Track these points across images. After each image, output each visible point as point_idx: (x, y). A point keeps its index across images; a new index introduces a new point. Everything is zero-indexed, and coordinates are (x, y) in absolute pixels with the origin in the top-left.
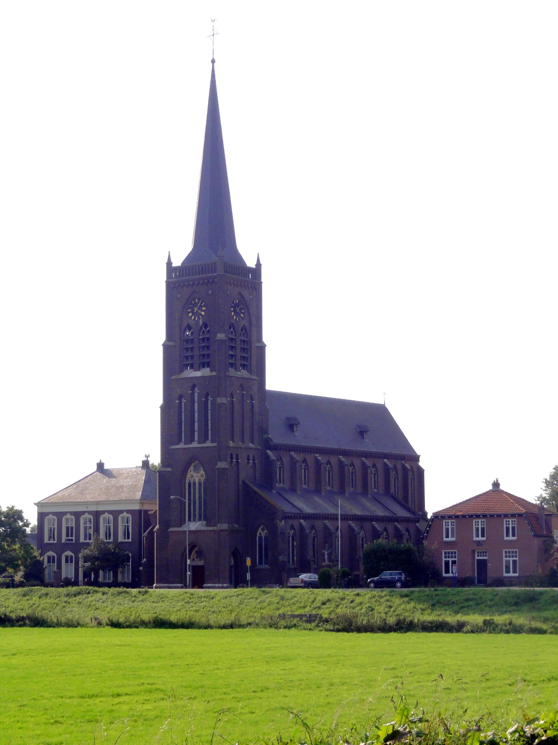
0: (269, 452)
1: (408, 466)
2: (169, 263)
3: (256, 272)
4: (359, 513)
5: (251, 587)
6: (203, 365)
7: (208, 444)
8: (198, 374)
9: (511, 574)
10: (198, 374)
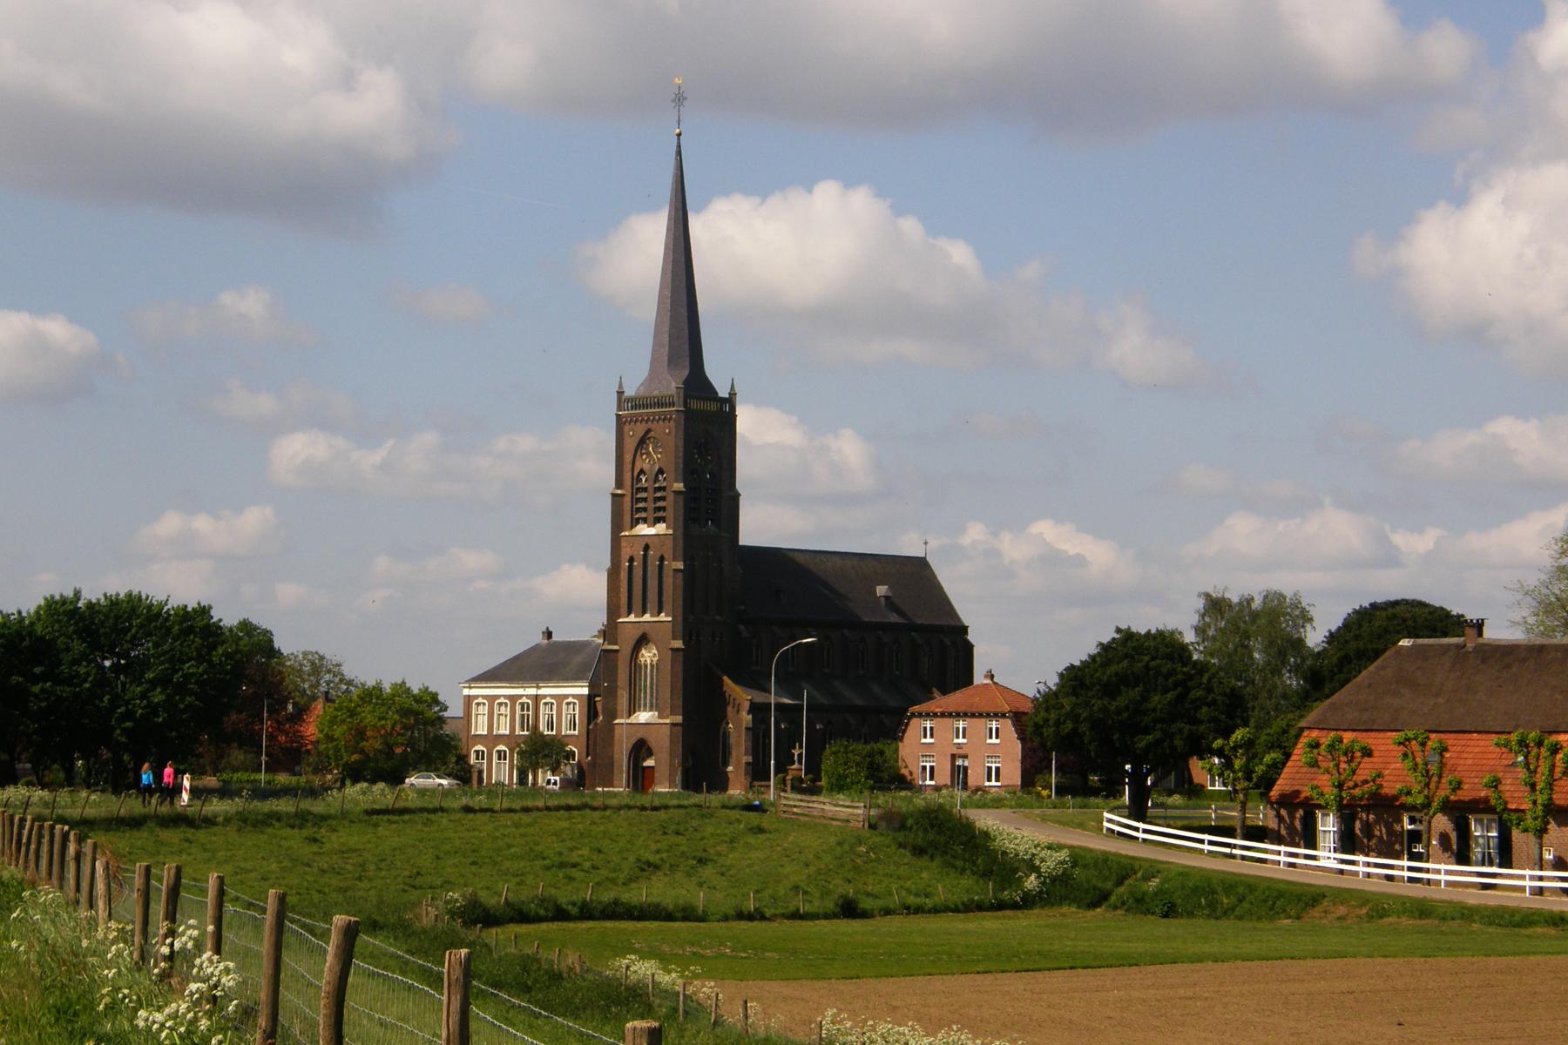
0: (742, 627)
1: (947, 641)
2: (620, 393)
3: (731, 401)
4: (859, 702)
5: (708, 791)
6: (658, 520)
7: (663, 617)
8: (652, 531)
9: (993, 783)
10: (652, 531)
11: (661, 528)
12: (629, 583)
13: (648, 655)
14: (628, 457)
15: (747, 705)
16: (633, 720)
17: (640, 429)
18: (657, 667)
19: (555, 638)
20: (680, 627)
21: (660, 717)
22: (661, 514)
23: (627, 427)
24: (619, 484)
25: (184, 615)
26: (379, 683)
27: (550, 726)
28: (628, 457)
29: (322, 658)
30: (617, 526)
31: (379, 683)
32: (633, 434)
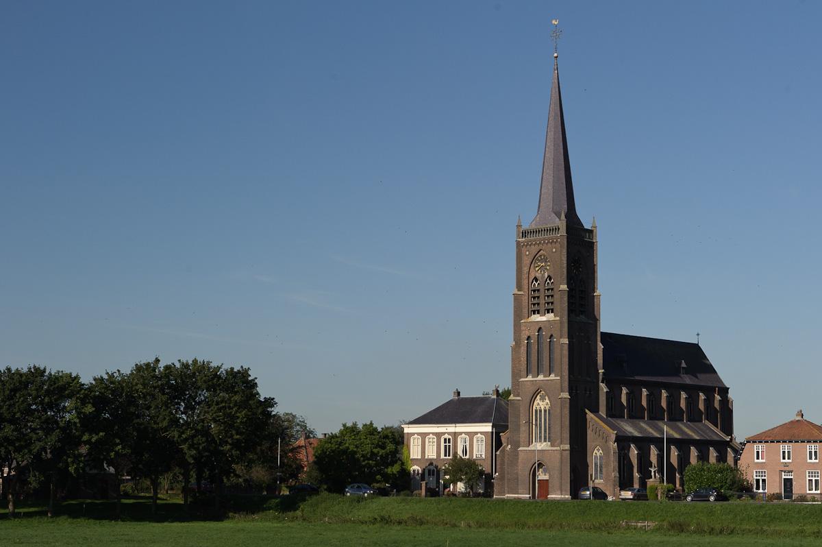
2: (519, 226)
4: (637, 434)
8: (544, 318)
10: (544, 318)
11: (550, 316)
12: (531, 355)
13: (541, 404)
14: (525, 270)
15: (613, 437)
16: (532, 448)
17: (534, 249)
18: (549, 412)
19: (461, 396)
20: (566, 384)
21: (552, 446)
22: (550, 307)
23: (524, 249)
24: (519, 287)
25: (231, 373)
26: (355, 424)
27: (465, 451)
28: (525, 270)
29: (294, 417)
30: (518, 316)
31: (355, 424)
32: (528, 254)
